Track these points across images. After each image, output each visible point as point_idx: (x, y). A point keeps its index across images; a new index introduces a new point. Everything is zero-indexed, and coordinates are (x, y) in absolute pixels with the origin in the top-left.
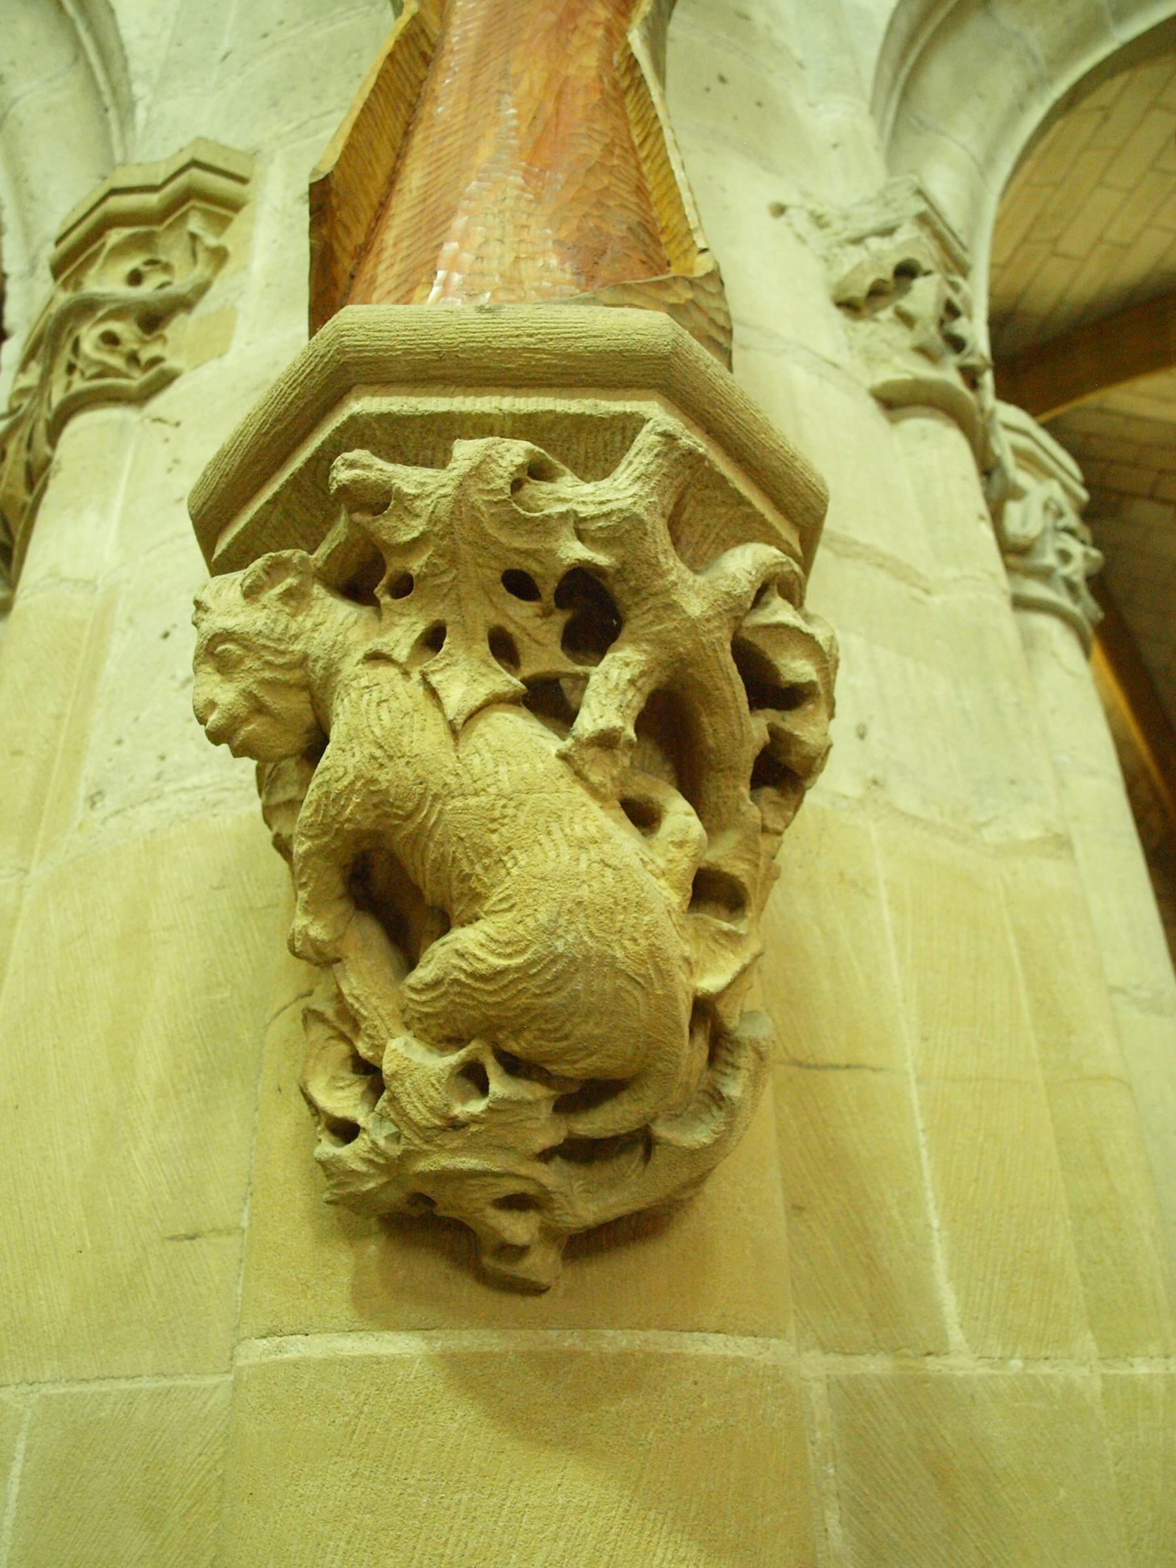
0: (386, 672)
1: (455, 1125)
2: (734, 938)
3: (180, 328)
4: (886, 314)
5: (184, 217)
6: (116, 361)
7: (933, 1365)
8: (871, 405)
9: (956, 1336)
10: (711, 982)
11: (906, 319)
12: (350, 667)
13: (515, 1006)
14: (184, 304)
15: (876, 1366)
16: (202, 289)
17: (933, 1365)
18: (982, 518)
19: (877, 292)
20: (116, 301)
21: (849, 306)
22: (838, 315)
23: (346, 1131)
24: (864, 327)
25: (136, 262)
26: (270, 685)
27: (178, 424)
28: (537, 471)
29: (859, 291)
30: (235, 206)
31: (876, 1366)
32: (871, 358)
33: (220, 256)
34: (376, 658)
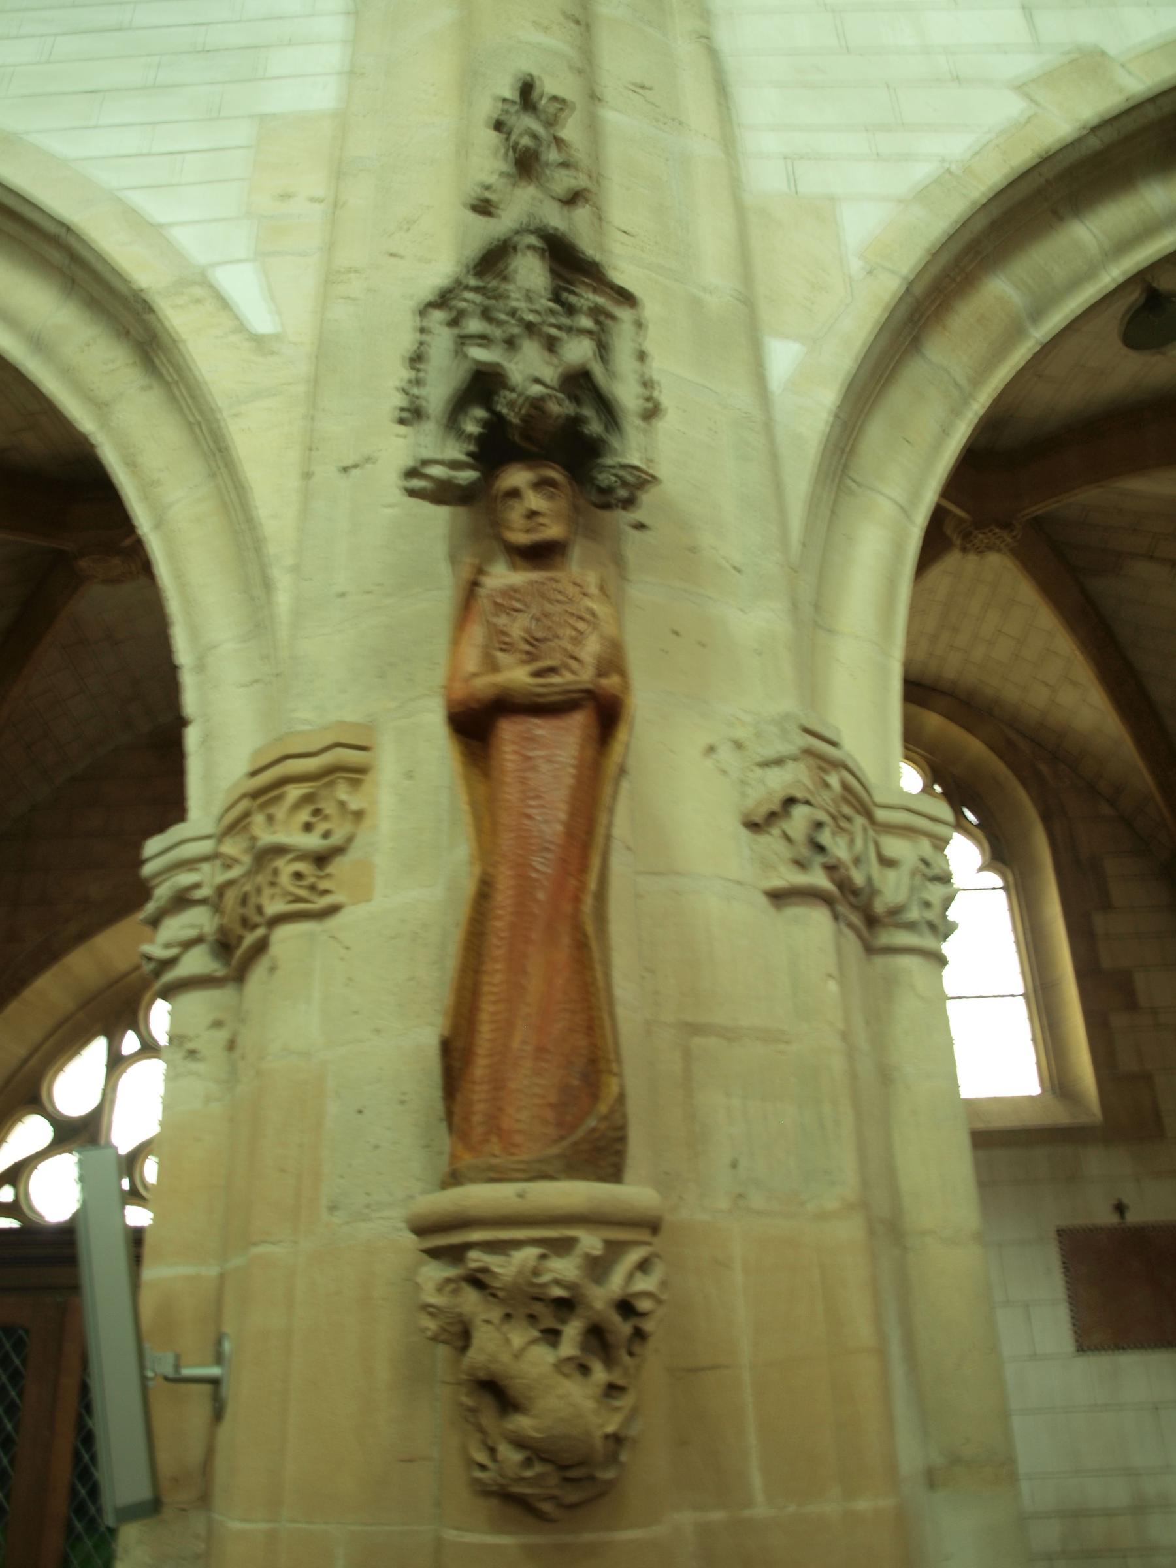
0: (489, 1327)
1: (523, 1479)
2: (618, 1409)
3: (337, 867)
4: (776, 831)
5: (332, 784)
6: (303, 893)
7: (747, 1513)
8: (764, 901)
9: (759, 1497)
10: (610, 1429)
11: (787, 838)
12: (478, 1322)
13: (539, 1468)
14: (339, 851)
15: (717, 1516)
16: (350, 839)
17: (747, 1513)
18: (830, 976)
19: (772, 816)
20: (299, 850)
21: (753, 826)
22: (745, 833)
23: (483, 1467)
24: (764, 839)
25: (304, 816)
26: (449, 1324)
27: (347, 948)
28: (543, 1257)
29: (758, 817)
30: (362, 770)
31: (717, 1516)
32: (766, 866)
33: (359, 815)
34: (488, 1322)
